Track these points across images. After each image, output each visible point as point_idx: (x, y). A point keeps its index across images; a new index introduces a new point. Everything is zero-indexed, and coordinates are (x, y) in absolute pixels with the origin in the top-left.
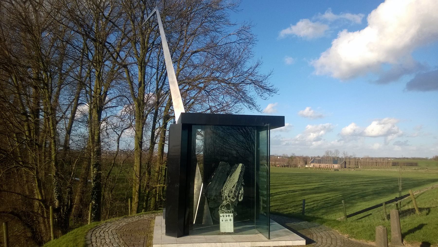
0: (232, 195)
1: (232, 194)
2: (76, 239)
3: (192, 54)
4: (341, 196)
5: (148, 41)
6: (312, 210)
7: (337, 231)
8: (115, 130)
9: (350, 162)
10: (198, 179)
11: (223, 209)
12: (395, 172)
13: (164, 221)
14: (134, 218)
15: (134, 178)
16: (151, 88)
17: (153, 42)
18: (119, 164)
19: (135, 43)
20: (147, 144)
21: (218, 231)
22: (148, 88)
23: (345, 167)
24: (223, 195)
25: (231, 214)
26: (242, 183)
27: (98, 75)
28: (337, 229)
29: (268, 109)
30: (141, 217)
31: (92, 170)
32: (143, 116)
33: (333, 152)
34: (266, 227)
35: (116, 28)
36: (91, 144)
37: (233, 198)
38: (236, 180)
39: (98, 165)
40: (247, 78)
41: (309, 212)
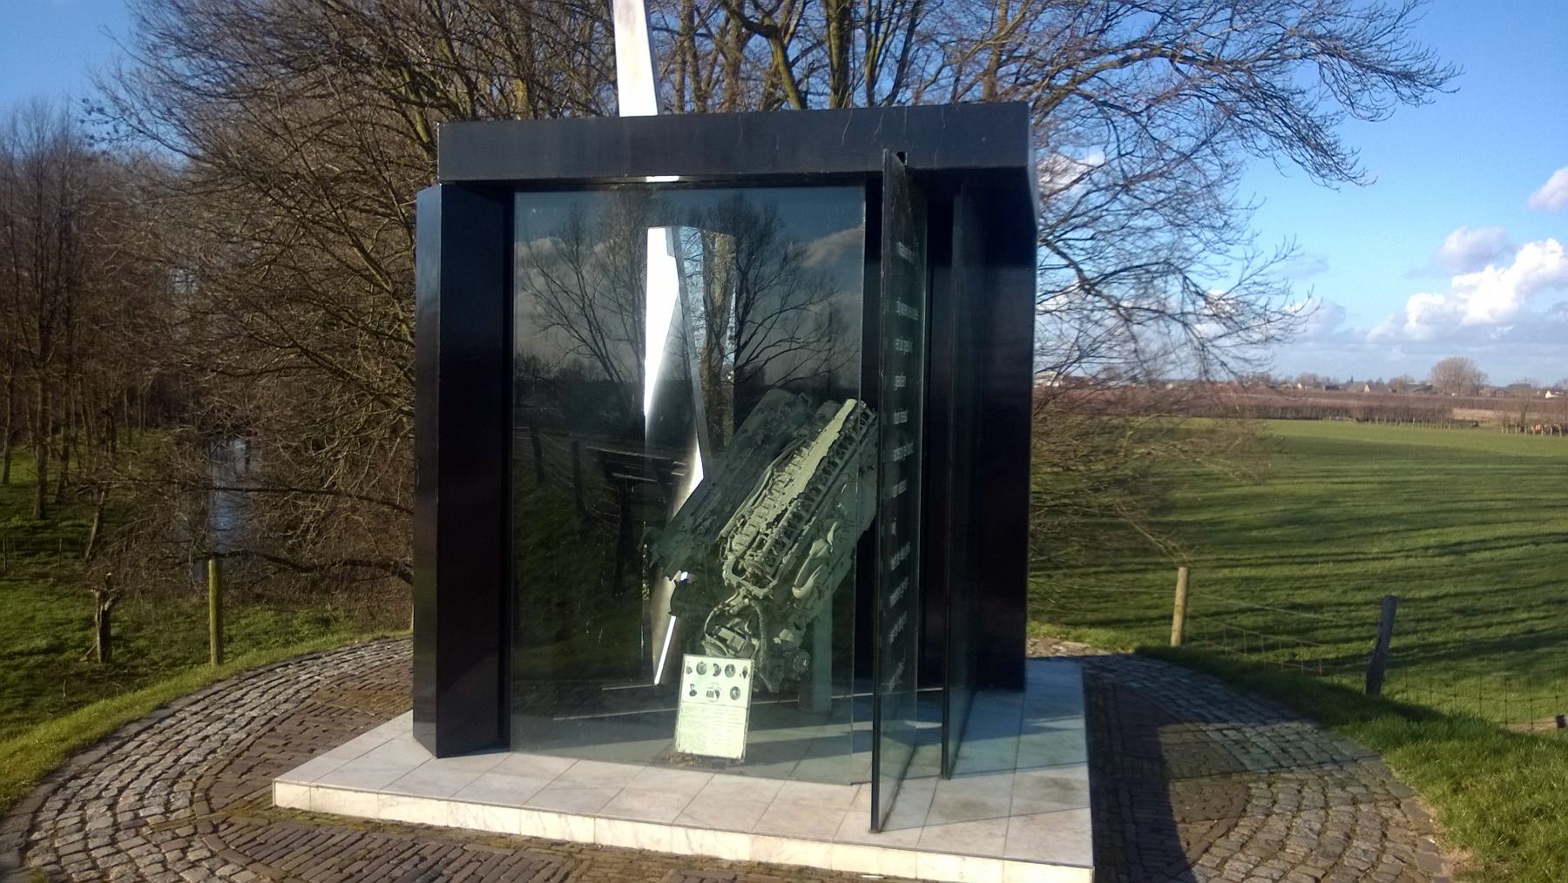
11: (724, 633)
21: (655, 746)
28: (1434, 801)
38: (799, 486)
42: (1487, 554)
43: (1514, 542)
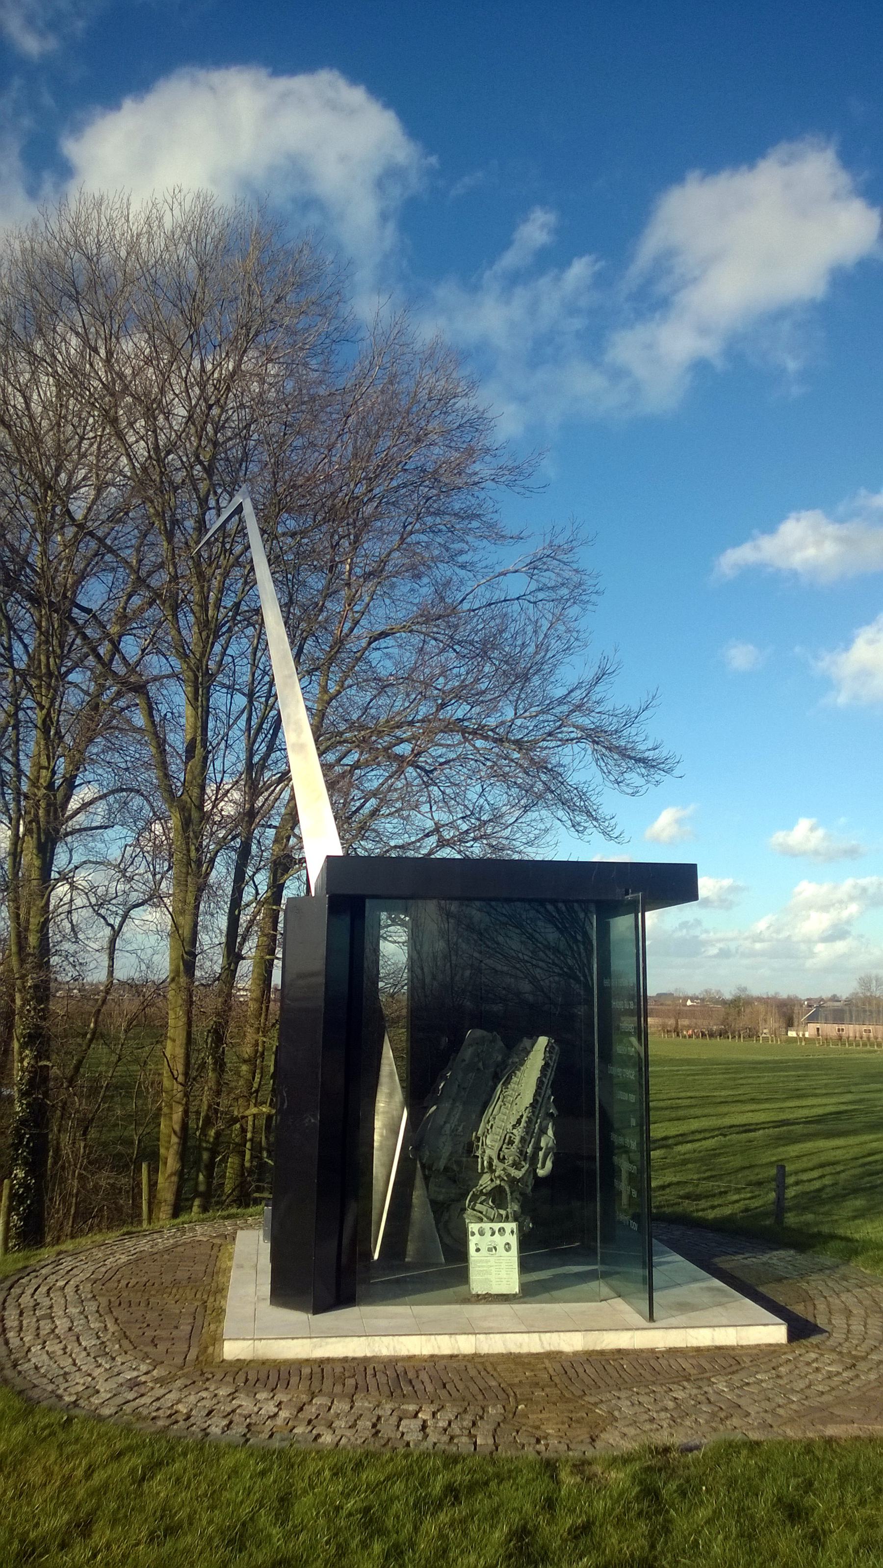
0: (511, 1153)
1: (514, 1149)
3: (370, 643)
5: (219, 600)
6: (814, 1200)
8: (102, 911)
10: (391, 1095)
11: (478, 1207)
14: (161, 1236)
15: (166, 1083)
16: (229, 762)
17: (237, 605)
18: (113, 1032)
19: (175, 608)
20: (211, 961)
21: (461, 1289)
22: (218, 764)
24: (479, 1153)
27: (44, 721)
29: (640, 830)
31: (16, 1056)
32: (199, 863)
34: (640, 1272)
35: (109, 557)
36: (14, 962)
37: (516, 1165)
38: (528, 1098)
39: (37, 1039)
40: (562, 722)
41: (805, 1209)
42: (689, 1146)
43: (707, 1135)
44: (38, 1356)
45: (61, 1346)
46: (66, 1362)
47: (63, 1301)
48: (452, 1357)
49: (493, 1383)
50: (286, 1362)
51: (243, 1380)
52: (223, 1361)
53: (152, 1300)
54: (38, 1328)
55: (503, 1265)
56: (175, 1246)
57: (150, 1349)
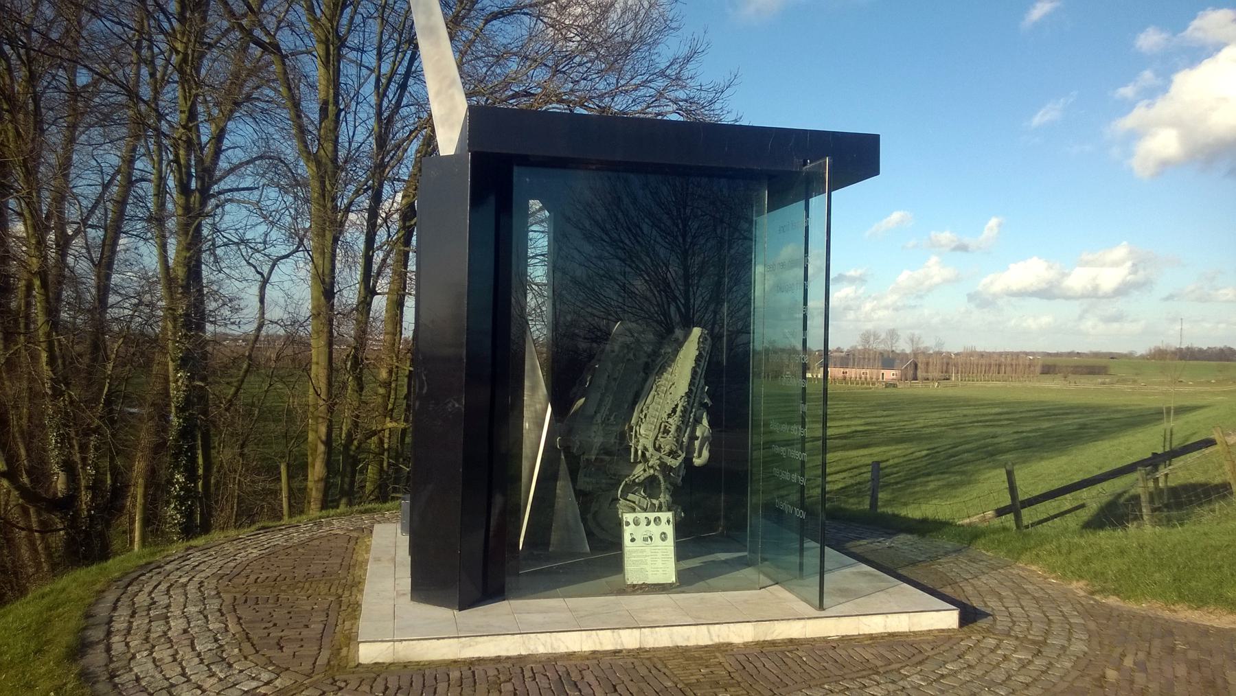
0: (668, 443)
1: (670, 437)
2: (49, 620)
4: (924, 453)
7: (1034, 568)
9: (927, 364)
11: (631, 496)
12: (1051, 390)
13: (404, 541)
14: (297, 532)
21: (615, 578)
23: (915, 378)
25: (666, 516)
26: (702, 398)
30: (320, 526)
33: (883, 336)
37: (672, 454)
38: (683, 387)
44: (142, 666)
45: (171, 651)
46: (173, 672)
47: (182, 600)
48: (616, 652)
49: (669, 684)
50: (430, 664)
51: (383, 688)
52: (359, 664)
53: (282, 596)
54: (149, 631)
55: (659, 555)
56: (311, 539)
57: (274, 653)
